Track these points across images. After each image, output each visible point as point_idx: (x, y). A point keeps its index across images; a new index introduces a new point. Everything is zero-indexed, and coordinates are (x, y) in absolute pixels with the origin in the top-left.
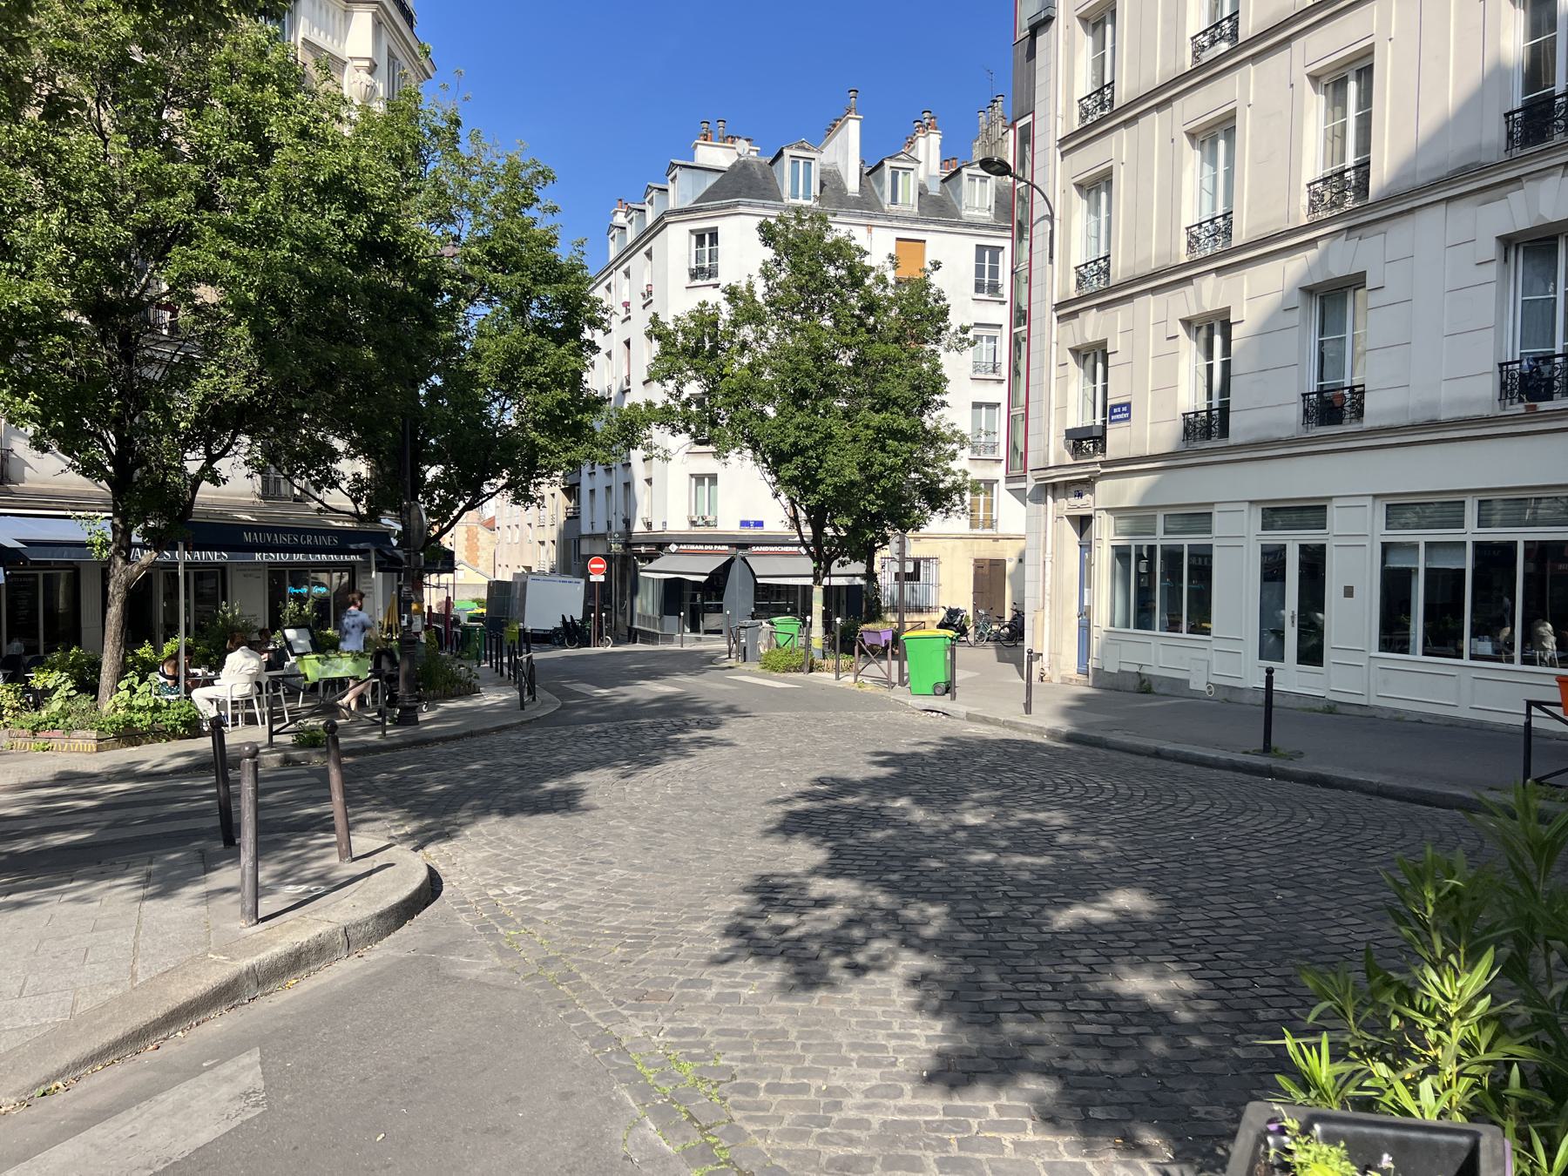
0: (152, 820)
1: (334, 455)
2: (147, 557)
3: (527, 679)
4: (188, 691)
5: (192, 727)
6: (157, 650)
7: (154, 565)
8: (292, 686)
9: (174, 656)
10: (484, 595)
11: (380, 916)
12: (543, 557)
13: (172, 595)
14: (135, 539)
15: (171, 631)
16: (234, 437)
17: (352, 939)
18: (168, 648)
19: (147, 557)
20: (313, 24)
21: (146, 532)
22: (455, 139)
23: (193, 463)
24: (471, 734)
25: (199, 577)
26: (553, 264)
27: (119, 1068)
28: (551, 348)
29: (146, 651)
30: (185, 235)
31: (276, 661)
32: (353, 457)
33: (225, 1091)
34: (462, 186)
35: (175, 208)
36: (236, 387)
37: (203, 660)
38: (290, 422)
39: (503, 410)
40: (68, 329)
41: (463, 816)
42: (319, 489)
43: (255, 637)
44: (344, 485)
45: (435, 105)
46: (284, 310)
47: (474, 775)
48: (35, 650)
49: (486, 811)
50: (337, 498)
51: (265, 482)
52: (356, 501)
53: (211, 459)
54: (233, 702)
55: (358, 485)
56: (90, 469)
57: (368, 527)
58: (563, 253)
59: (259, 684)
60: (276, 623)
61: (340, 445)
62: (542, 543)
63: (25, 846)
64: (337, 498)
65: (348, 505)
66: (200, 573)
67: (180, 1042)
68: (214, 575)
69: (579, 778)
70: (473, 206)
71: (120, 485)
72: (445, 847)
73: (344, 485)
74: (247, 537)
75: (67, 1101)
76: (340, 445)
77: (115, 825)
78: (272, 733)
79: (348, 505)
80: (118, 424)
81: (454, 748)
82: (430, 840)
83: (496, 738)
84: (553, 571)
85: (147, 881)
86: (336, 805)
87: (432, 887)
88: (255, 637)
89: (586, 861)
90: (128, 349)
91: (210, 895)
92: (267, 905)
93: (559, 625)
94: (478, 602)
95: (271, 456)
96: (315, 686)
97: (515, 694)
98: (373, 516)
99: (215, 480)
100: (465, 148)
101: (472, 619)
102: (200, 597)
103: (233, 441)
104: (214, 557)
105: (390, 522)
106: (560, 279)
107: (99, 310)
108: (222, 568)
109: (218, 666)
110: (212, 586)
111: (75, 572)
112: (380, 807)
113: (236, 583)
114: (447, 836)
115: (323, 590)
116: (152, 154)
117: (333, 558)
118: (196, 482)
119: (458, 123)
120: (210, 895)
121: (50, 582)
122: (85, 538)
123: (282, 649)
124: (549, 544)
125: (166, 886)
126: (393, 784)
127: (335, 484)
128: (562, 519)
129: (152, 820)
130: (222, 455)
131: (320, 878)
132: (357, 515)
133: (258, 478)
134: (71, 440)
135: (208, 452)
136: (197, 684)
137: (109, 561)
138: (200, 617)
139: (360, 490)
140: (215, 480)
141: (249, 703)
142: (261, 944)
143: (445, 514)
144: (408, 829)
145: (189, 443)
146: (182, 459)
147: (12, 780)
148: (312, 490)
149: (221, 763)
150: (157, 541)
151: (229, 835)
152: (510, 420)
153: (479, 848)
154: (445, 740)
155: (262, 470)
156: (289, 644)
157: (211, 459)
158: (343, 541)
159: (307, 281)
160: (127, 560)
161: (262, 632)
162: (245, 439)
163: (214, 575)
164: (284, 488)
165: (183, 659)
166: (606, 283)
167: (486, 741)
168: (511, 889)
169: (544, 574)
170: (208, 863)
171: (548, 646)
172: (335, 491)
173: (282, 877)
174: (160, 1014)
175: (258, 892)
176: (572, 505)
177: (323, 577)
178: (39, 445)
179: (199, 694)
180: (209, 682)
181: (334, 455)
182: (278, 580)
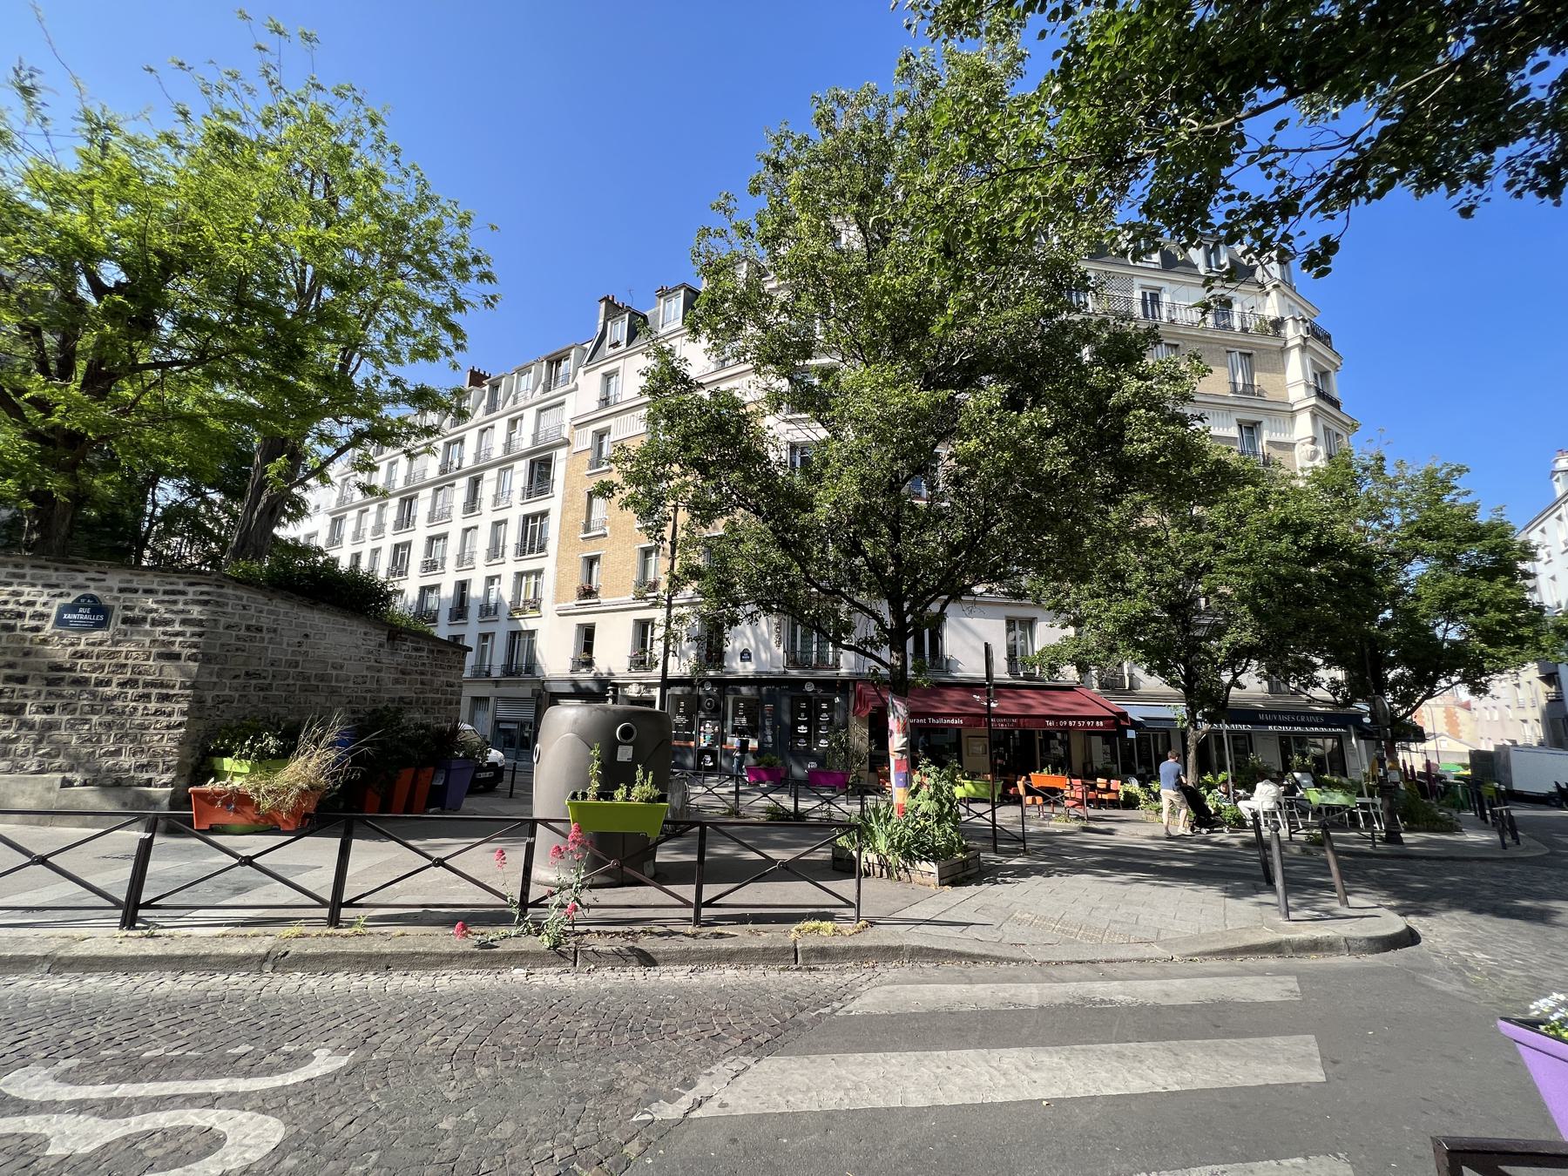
0: (1224, 865)
1: (1315, 667)
2: (1205, 727)
3: (1508, 827)
4: (1235, 802)
5: (1239, 822)
6: (1215, 778)
7: (1209, 732)
8: (1304, 808)
9: (1225, 782)
10: (1467, 761)
11: (1370, 939)
12: (1528, 733)
13: (1220, 747)
14: (1198, 717)
15: (1222, 768)
16: (1248, 661)
17: (1350, 946)
18: (1221, 777)
19: (1205, 727)
20: (1271, 431)
21: (1204, 715)
22: (1381, 468)
23: (1226, 677)
24: (1453, 859)
25: (1235, 738)
26: (1477, 527)
27: (1219, 963)
28: (1484, 585)
29: (1208, 778)
30: (1209, 568)
31: (1291, 790)
32: (1328, 668)
33: (1279, 986)
34: (1389, 495)
35: (1203, 556)
36: (1247, 637)
37: (1243, 786)
38: (1282, 650)
39: (1446, 630)
40: (1156, 620)
41: (1438, 905)
42: (1306, 688)
43: (1275, 776)
44: (1324, 685)
45: (1360, 449)
46: (1269, 594)
47: (1452, 884)
48: (1151, 772)
49: (1461, 907)
50: (1320, 693)
51: (1270, 685)
52: (1334, 695)
53: (1236, 675)
54: (1265, 813)
55: (1335, 686)
56: (1173, 684)
57: (1341, 711)
58: (1483, 518)
59: (1279, 803)
60: (1287, 768)
61: (1319, 661)
62: (1525, 721)
63: (1162, 863)
64: (1320, 693)
65: (1329, 697)
66: (1236, 737)
67: (1252, 961)
68: (1242, 738)
69: (1555, 904)
70: (1401, 504)
71: (1189, 691)
72: (1424, 920)
73: (1324, 685)
74: (1261, 717)
75: (1200, 965)
76: (1319, 661)
77: (1204, 863)
78: (1290, 833)
79: (1329, 697)
80: (1184, 661)
81: (1437, 865)
82: (1412, 913)
83: (1477, 865)
84: (1541, 744)
85: (1226, 890)
86: (1335, 878)
87: (1409, 938)
88: (1275, 776)
89: (1554, 956)
90: (1187, 627)
91: (1261, 904)
92: (1293, 915)
93: (1554, 790)
94: (1465, 766)
95: (1272, 671)
96: (1319, 810)
97: (1496, 837)
98: (1348, 703)
99: (1240, 686)
100: (1390, 472)
101: (1458, 778)
102: (1236, 750)
103: (1247, 664)
104: (1243, 727)
105: (1362, 706)
106: (1480, 538)
107: (1171, 608)
108: (1249, 734)
109: (1252, 790)
110: (1243, 745)
111: (1168, 732)
112: (1373, 887)
113: (1257, 741)
114: (1426, 914)
115: (1318, 750)
116: (1189, 533)
117: (1323, 729)
118: (1228, 689)
119: (1383, 459)
120: (1261, 904)
121: (1155, 737)
122: (1173, 716)
123: (1293, 785)
124: (1532, 722)
125: (1237, 894)
126: (1381, 877)
127: (1318, 685)
128: (1544, 702)
129: (1224, 865)
130: (1242, 672)
131: (1327, 911)
132: (1336, 702)
133: (1265, 683)
134: (1163, 670)
135: (1233, 671)
136: (1240, 798)
137: (1187, 728)
138: (1237, 762)
139: (1336, 688)
140: (1240, 686)
141: (1274, 814)
142: (1291, 931)
143: (1407, 700)
144: (1393, 903)
145: (1223, 667)
146: (1218, 675)
147: (1149, 833)
148: (1302, 689)
149: (1260, 844)
150: (1211, 718)
151: (1270, 881)
152: (1454, 635)
153: (1452, 926)
154: (1428, 858)
155: (1266, 678)
156: (1298, 782)
157: (1236, 675)
158: (1328, 719)
159: (1279, 578)
160: (1196, 728)
161: (1278, 773)
162: (1255, 662)
163: (1242, 738)
164: (1283, 687)
165: (1231, 784)
166: (1540, 527)
167: (1468, 865)
168: (1480, 956)
169: (1530, 746)
170: (1258, 891)
171: (1543, 806)
172: (1318, 689)
173: (1302, 906)
174: (1241, 945)
175: (1288, 909)
176: (1553, 689)
177: (1320, 741)
178: (1149, 672)
179: (1241, 804)
180: (1247, 798)
181: (1315, 667)
182: (1287, 745)
